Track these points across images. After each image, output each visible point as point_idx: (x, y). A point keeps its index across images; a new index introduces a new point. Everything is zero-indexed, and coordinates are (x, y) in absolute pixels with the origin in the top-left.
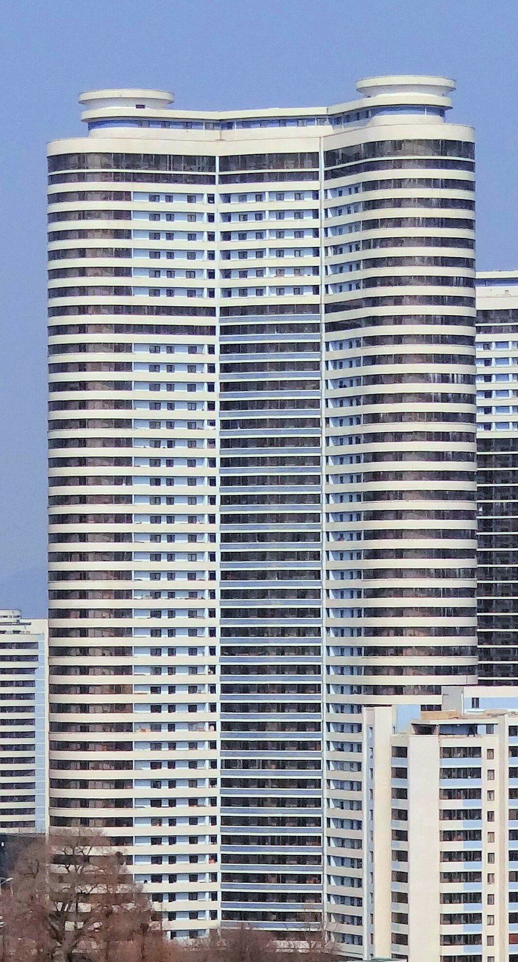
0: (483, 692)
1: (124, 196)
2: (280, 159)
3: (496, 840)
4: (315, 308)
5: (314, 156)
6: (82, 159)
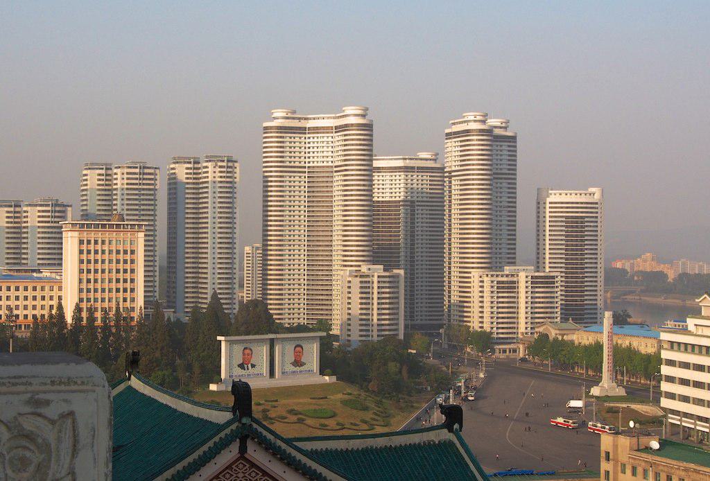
0: (371, 267)
1: (283, 137)
2: (323, 128)
3: (386, 158)
4: (332, 167)
5: (332, 127)
6: (271, 128)
